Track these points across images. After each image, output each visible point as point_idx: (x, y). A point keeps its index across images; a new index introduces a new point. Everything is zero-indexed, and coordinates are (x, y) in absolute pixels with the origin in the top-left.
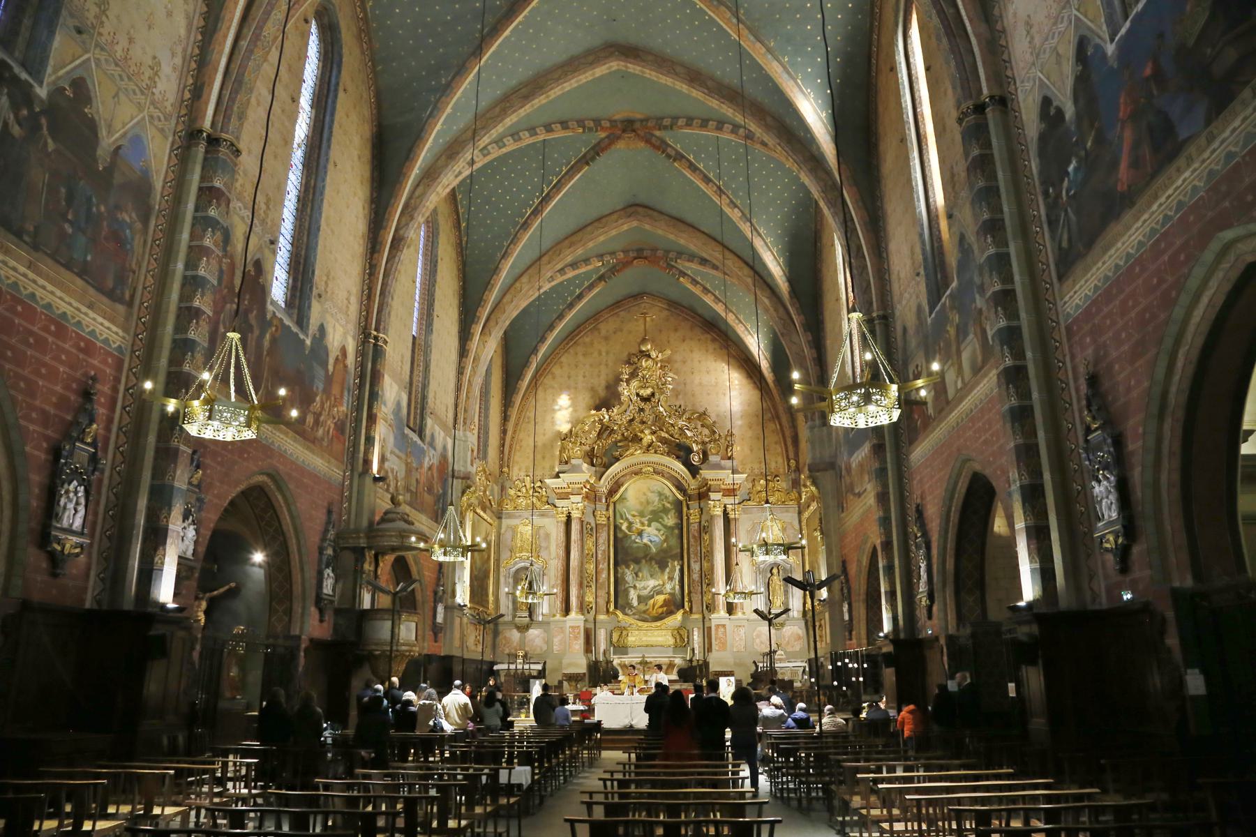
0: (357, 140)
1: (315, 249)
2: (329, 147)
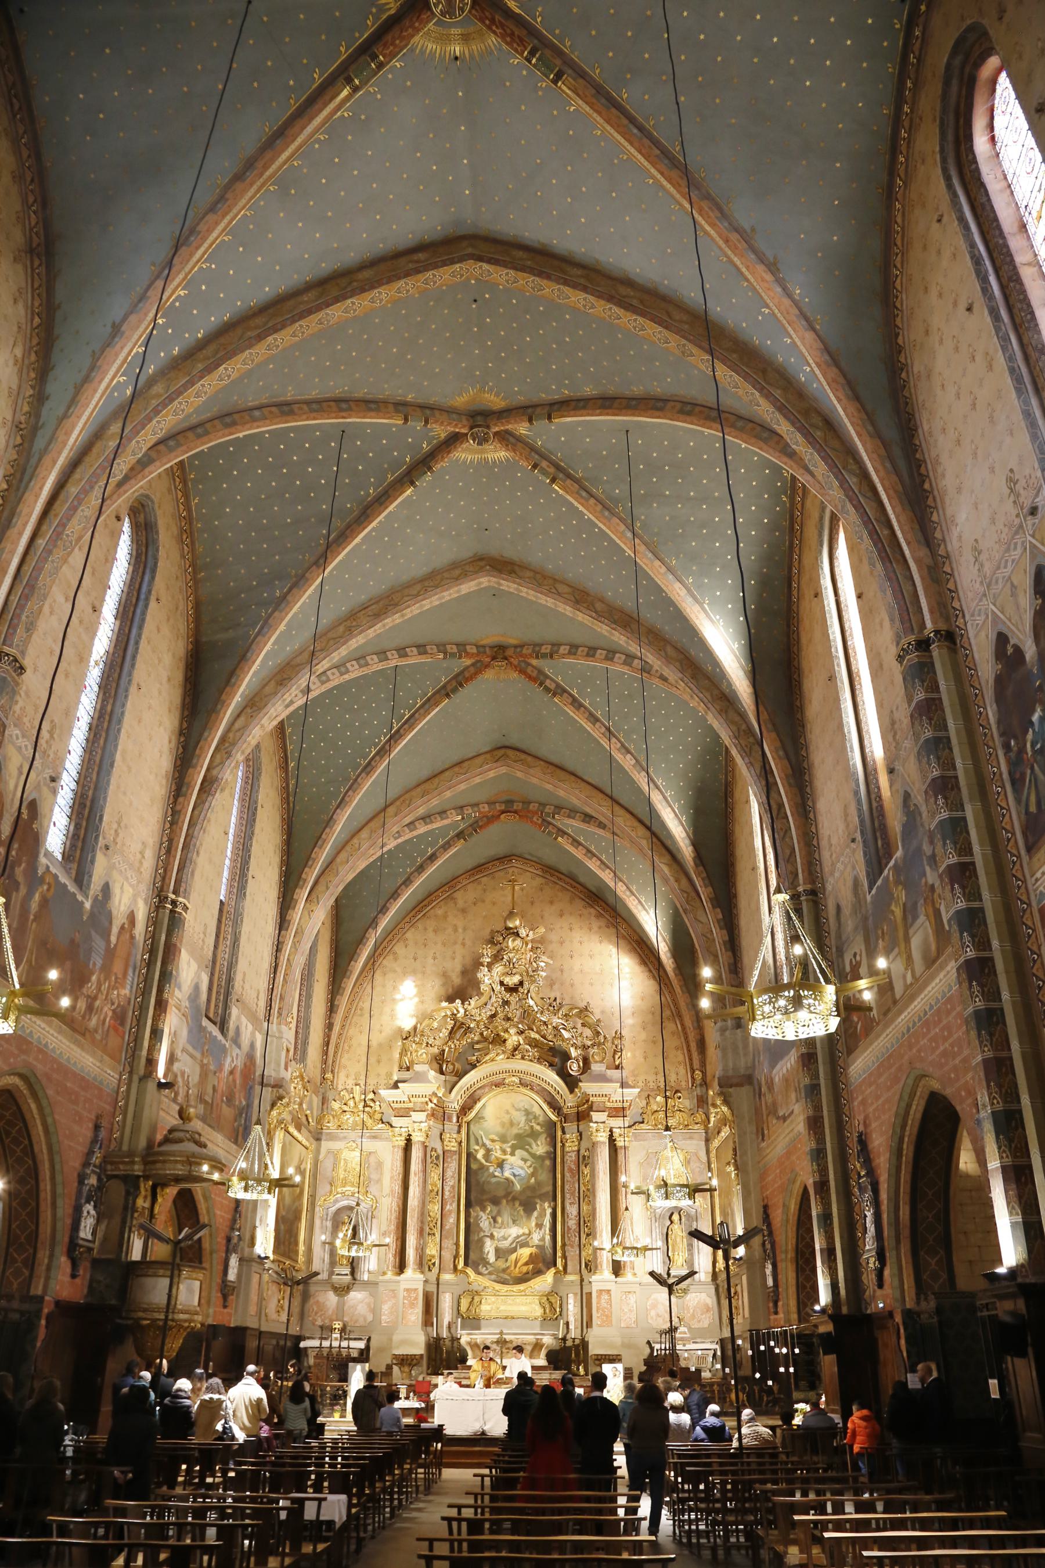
2: (133, 666)
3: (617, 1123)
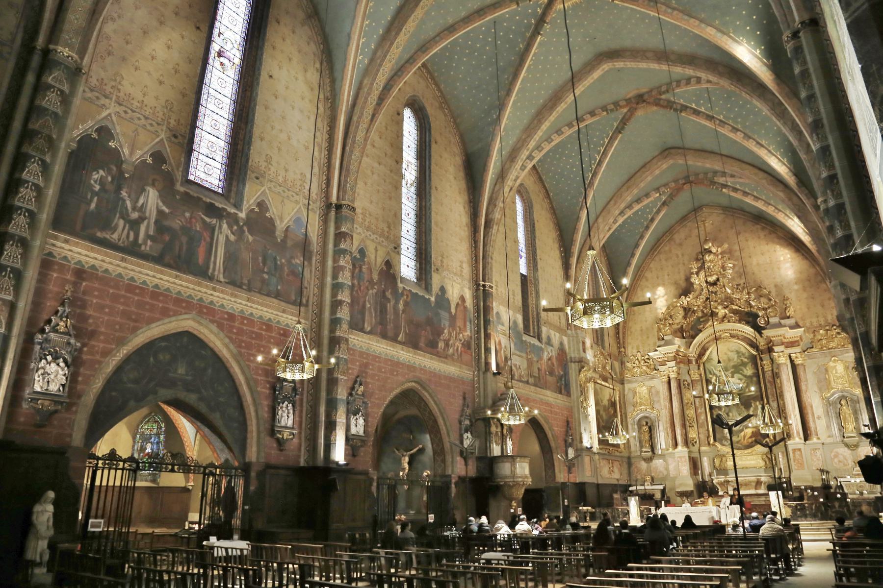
0: (451, 169)
1: (430, 244)
2: (430, 179)
3: (794, 351)
